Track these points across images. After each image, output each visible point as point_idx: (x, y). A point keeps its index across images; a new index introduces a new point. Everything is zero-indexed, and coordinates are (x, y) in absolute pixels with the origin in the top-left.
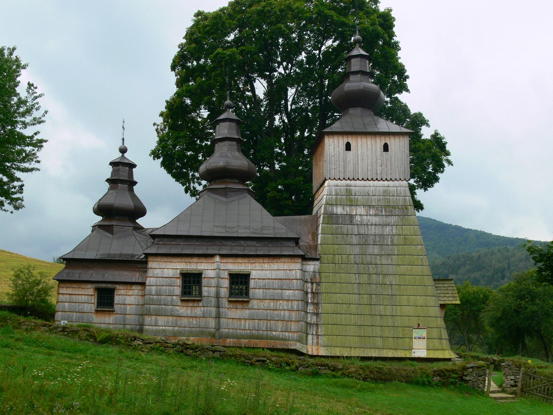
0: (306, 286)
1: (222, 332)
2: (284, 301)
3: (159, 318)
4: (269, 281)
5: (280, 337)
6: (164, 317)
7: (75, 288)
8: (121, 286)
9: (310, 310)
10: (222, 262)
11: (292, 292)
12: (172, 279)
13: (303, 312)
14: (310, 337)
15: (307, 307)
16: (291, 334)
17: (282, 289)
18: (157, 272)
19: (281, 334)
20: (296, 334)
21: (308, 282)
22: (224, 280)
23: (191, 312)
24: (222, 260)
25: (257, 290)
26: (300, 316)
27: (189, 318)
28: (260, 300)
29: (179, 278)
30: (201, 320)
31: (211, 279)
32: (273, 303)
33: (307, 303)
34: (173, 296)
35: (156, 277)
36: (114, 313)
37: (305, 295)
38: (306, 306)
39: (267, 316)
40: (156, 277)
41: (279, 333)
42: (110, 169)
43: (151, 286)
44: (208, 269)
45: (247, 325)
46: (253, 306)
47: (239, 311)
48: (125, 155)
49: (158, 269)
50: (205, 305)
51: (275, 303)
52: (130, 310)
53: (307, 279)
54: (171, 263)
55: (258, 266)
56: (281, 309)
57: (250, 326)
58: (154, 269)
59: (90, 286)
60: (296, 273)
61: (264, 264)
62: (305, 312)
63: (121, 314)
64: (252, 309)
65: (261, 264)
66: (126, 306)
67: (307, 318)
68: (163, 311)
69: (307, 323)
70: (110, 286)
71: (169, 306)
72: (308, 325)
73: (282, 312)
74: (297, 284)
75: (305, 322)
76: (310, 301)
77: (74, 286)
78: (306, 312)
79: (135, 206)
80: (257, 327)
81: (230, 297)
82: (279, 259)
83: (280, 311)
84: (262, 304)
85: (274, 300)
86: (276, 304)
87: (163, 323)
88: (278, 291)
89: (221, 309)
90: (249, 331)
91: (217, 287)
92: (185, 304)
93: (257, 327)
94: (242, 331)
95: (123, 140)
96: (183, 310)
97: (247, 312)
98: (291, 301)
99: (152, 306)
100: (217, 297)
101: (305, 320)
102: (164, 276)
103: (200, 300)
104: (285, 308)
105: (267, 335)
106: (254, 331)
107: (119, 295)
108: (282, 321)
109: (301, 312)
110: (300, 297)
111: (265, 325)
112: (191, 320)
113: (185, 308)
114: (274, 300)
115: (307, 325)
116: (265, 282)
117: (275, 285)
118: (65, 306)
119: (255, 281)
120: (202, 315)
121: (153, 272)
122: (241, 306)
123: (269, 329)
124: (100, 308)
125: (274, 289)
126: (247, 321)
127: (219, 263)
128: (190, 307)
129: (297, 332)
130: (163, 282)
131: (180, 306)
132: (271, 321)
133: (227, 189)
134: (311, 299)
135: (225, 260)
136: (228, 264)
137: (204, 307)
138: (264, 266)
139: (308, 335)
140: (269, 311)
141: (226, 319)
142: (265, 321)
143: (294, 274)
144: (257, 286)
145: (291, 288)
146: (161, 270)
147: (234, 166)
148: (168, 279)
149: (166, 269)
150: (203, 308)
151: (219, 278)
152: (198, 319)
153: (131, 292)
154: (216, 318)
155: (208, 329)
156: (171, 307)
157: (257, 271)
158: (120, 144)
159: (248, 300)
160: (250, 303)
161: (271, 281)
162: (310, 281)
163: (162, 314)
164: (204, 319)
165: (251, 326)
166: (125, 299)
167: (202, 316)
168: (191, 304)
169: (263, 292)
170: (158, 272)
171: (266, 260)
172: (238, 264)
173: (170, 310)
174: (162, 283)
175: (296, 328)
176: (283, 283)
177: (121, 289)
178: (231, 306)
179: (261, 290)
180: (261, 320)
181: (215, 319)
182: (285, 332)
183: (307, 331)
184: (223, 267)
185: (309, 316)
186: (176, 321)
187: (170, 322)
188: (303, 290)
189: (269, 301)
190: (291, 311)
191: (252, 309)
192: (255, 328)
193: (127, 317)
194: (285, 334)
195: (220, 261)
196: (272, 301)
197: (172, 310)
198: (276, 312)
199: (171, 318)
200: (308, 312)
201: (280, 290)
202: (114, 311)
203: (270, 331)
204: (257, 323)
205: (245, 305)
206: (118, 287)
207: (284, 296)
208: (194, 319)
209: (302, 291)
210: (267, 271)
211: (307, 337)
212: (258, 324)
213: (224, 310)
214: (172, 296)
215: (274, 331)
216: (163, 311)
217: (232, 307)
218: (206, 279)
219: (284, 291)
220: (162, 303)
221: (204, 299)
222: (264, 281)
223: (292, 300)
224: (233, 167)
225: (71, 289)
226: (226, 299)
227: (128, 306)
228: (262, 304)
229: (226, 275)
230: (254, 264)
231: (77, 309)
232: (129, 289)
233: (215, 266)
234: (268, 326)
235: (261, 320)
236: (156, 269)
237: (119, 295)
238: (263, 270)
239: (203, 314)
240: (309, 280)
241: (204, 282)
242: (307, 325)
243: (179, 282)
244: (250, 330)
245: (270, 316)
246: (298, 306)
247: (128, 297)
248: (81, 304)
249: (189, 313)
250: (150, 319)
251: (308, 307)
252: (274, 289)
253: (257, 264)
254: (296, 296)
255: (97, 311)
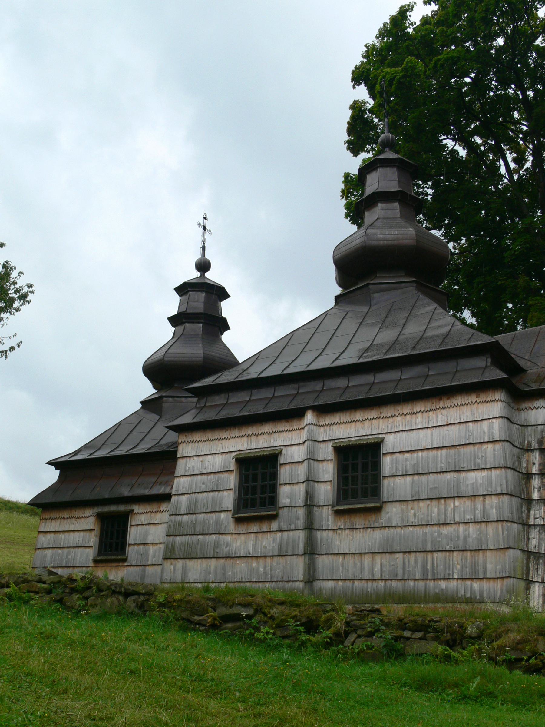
0: (528, 461)
1: (321, 589)
2: (465, 499)
3: (190, 564)
4: (425, 453)
5: (460, 595)
6: (200, 561)
7: (64, 518)
8: (141, 507)
9: (535, 518)
10: (321, 424)
11: (484, 473)
12: (220, 475)
13: (516, 526)
14: (537, 588)
15: (529, 511)
16: (486, 585)
17: (459, 471)
18: (193, 464)
19: (460, 586)
20: (499, 584)
21: (532, 450)
22: (325, 464)
23: (255, 545)
24: (320, 419)
25: (398, 480)
26: (508, 535)
27: (250, 560)
28: (405, 503)
29: (281, 484)
30: (274, 564)
31: (297, 465)
32: (439, 509)
33: (529, 501)
34: (221, 511)
35: (191, 475)
36: (126, 564)
37: (523, 482)
38: (524, 509)
39: (425, 542)
40: (191, 475)
41: (455, 582)
42: (177, 298)
43: (180, 495)
44: (292, 445)
45: (377, 568)
46: (389, 519)
47: (358, 535)
48: (207, 275)
49: (195, 458)
50: (284, 527)
51: (442, 507)
52: (154, 556)
53: (529, 443)
54: (220, 441)
55: (400, 423)
56: (457, 520)
57: (384, 569)
58: (188, 459)
59: (89, 512)
60: (490, 427)
61: (414, 415)
62: (524, 525)
63: (137, 566)
64: (389, 527)
65: (408, 417)
66: (147, 547)
67: (528, 539)
68: (199, 546)
69: (528, 553)
70: (122, 508)
71: (211, 537)
72: (532, 557)
73: (461, 528)
74: (494, 455)
75: (523, 551)
76: (536, 496)
77: (64, 516)
78: (527, 526)
79: (204, 357)
80: (400, 571)
81: (338, 503)
82: (447, 399)
83: (455, 527)
84: (412, 512)
85: (439, 499)
86: (445, 510)
87: (198, 575)
88: (448, 476)
89: (319, 534)
90: (382, 584)
91: (308, 480)
92: (243, 528)
93: (400, 571)
94: (365, 585)
95: (204, 248)
96: (239, 544)
97: (378, 535)
98: (481, 498)
99: (178, 539)
100: (306, 505)
101: (522, 546)
102: (205, 471)
103: (274, 517)
104: (468, 517)
105: (425, 592)
106: (394, 584)
107: (137, 525)
108: (461, 553)
109: (509, 524)
110: (504, 486)
111: (420, 564)
112: (254, 565)
113: (243, 537)
114: (439, 499)
115: (528, 559)
116: (417, 457)
117: (441, 462)
118: (45, 556)
119: (393, 460)
120: (277, 549)
121: (186, 465)
122: (363, 522)
123: (429, 574)
124: (115, 555)
125: (440, 472)
126: (378, 558)
127: (311, 427)
128: (252, 535)
129: (503, 578)
130: (203, 484)
131: (232, 533)
132: (435, 555)
133: (371, 286)
134: (539, 491)
135: (327, 420)
136: (335, 427)
137: (281, 531)
138: (414, 420)
139: (532, 586)
140: (428, 529)
141: (331, 557)
142: (420, 556)
143: (486, 430)
144: (397, 469)
145: (479, 466)
146: (201, 458)
147: (384, 240)
148: (212, 476)
149: (210, 457)
150: (279, 535)
151: (311, 461)
152: (269, 560)
153: (158, 518)
154: (305, 554)
155: (291, 583)
156: (214, 537)
157: (398, 435)
158: (198, 256)
159: (378, 505)
160: (383, 513)
161: (431, 453)
162: (536, 446)
163: (197, 554)
164: (281, 560)
165: (386, 569)
166: (146, 534)
167: (276, 554)
168: (254, 527)
169: (413, 482)
170: (194, 465)
171: (419, 406)
172: (355, 425)
173: (213, 545)
174: (200, 487)
175: (499, 567)
176: (459, 455)
177: (142, 513)
178: (340, 523)
179: (409, 479)
180: (409, 552)
181: (303, 557)
182: (472, 579)
183: (528, 573)
184: (322, 434)
185: (534, 533)
186: (224, 568)
187: (212, 571)
188: (514, 469)
189: (428, 502)
190: (483, 525)
191: (389, 527)
192: (397, 575)
193: (149, 570)
194: (471, 586)
195: (315, 422)
196: (435, 503)
197: (217, 545)
198: (445, 530)
199: (213, 562)
200: (532, 523)
201: (452, 474)
202: (125, 560)
203: (434, 579)
204: (402, 560)
205: (373, 517)
206: (136, 508)
207: (463, 488)
208: (261, 561)
209: (509, 471)
210: (420, 431)
211: (528, 588)
212: (404, 563)
213: (325, 534)
214: (217, 514)
215: (444, 579)
216: (199, 546)
217: (342, 527)
218: (288, 467)
219: (463, 474)
220: (198, 530)
221: (283, 513)
222: (415, 455)
223: (484, 496)
224: (382, 242)
225: (58, 522)
226: (330, 507)
227: (151, 547)
228: (412, 512)
229: (327, 451)
230: (391, 420)
231: (64, 562)
232: (156, 512)
233: (304, 435)
234: (429, 567)
235: (409, 552)
236: (192, 459)
237: (137, 525)
238: (413, 430)
239: (280, 549)
240: (534, 445)
241: (284, 473)
242: (528, 559)
243: (232, 480)
244: (386, 580)
245: (432, 542)
246: (499, 509)
247: (152, 529)
248: (72, 550)
249: (251, 549)
250: (172, 567)
251: (532, 512)
252: (440, 472)
253: (400, 418)
254: (494, 485)
255: (95, 561)
